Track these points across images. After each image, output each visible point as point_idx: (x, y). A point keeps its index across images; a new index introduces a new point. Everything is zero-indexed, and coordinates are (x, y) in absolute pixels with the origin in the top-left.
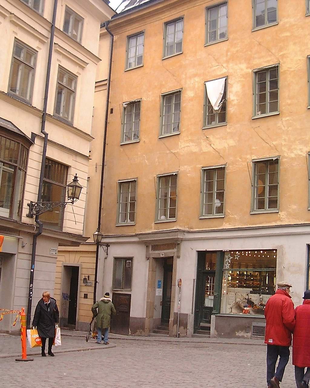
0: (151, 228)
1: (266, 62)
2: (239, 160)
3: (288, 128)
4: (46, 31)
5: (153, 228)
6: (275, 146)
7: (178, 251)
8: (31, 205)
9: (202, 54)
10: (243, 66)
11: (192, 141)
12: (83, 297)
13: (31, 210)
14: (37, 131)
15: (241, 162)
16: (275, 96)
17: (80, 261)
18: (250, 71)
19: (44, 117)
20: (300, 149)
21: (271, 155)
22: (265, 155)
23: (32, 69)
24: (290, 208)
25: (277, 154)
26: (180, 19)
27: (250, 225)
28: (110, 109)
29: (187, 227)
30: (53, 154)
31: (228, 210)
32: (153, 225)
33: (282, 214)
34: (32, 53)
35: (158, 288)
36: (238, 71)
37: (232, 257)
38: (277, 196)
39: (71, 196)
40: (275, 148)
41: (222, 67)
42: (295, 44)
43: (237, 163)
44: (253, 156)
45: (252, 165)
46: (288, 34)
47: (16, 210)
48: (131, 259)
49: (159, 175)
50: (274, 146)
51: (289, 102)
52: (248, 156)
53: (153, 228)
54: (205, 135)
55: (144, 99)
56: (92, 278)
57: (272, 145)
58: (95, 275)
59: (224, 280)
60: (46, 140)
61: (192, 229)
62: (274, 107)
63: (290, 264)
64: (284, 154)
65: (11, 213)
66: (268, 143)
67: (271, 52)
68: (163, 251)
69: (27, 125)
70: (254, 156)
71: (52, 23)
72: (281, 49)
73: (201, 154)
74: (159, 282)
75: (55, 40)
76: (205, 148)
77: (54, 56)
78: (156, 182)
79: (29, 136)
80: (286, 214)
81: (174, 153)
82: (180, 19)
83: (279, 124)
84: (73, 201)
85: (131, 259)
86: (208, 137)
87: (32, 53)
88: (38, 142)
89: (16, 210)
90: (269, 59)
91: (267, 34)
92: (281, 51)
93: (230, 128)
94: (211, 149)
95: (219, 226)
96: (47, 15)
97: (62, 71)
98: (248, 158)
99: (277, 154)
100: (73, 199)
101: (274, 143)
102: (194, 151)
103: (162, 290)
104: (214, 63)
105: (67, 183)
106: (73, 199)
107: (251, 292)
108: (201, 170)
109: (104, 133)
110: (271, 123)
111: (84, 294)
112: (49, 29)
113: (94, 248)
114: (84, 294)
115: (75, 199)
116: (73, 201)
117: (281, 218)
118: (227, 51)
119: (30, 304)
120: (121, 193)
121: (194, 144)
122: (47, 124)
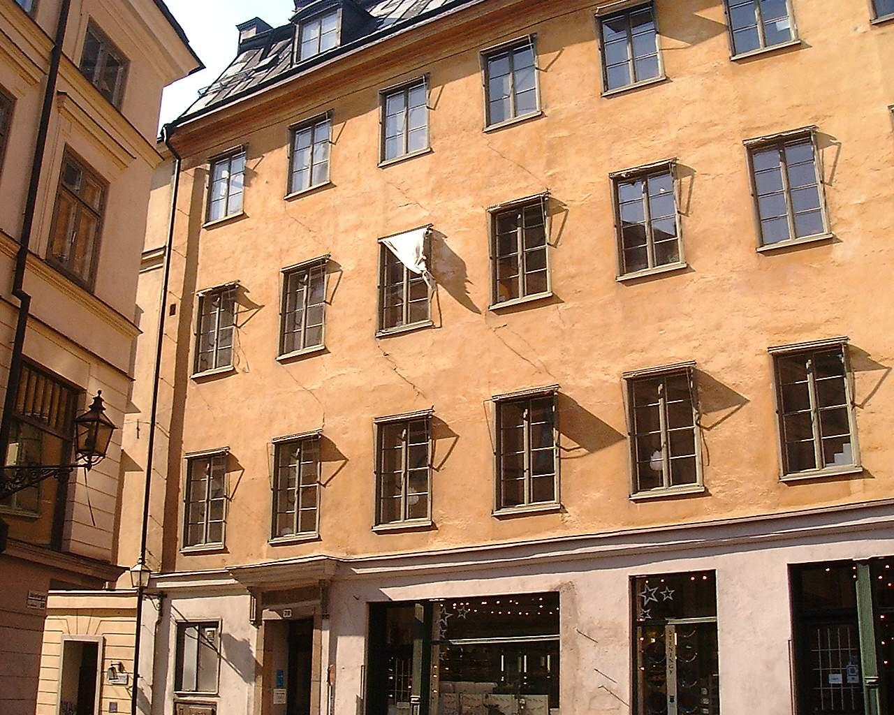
0: (260, 556)
1: (515, 191)
2: (461, 399)
3: (573, 325)
4: (42, 60)
5: (265, 554)
6: (545, 366)
7: (325, 605)
10: (466, 201)
11: (352, 363)
12: (108, 710)
15: (467, 404)
16: (537, 261)
17: (102, 630)
18: (482, 211)
20: (604, 369)
21: (537, 384)
22: (523, 384)
24: (586, 498)
25: (551, 381)
27: (492, 540)
28: (170, 306)
29: (344, 550)
31: (438, 511)
32: (266, 546)
35: (278, 687)
36: (454, 212)
37: (448, 622)
38: (559, 633)
39: (85, 448)
40: (545, 370)
41: (419, 206)
42: (578, 152)
43: (457, 406)
44: (495, 390)
45: (492, 407)
46: (564, 133)
48: (214, 624)
49: (277, 439)
50: (542, 365)
51: (573, 270)
52: (483, 391)
53: (265, 554)
54: (381, 350)
56: (129, 667)
57: (538, 364)
58: (137, 634)
59: (433, 666)
61: (354, 554)
62: (537, 282)
63: (593, 622)
64: (567, 381)
66: (528, 360)
67: (528, 171)
68: (291, 605)
70: (495, 388)
71: (56, 41)
72: (550, 163)
73: (374, 390)
74: (280, 673)
78: (271, 455)
80: (578, 512)
81: (310, 391)
84: (90, 462)
85: (214, 624)
86: (387, 353)
90: (524, 184)
92: (550, 169)
95: (420, 547)
97: (74, 167)
98: (481, 395)
99: (551, 381)
100: (90, 458)
101: (543, 358)
102: (357, 385)
103: (284, 691)
105: (78, 413)
106: (90, 458)
107: (496, 691)
108: (374, 424)
109: (151, 407)
111: (111, 703)
112: (46, 55)
113: (132, 603)
114: (111, 703)
115: (94, 458)
116: (90, 462)
117: (567, 521)
118: (430, 173)
119: (45, 113)
120: (202, 315)
121: (355, 370)
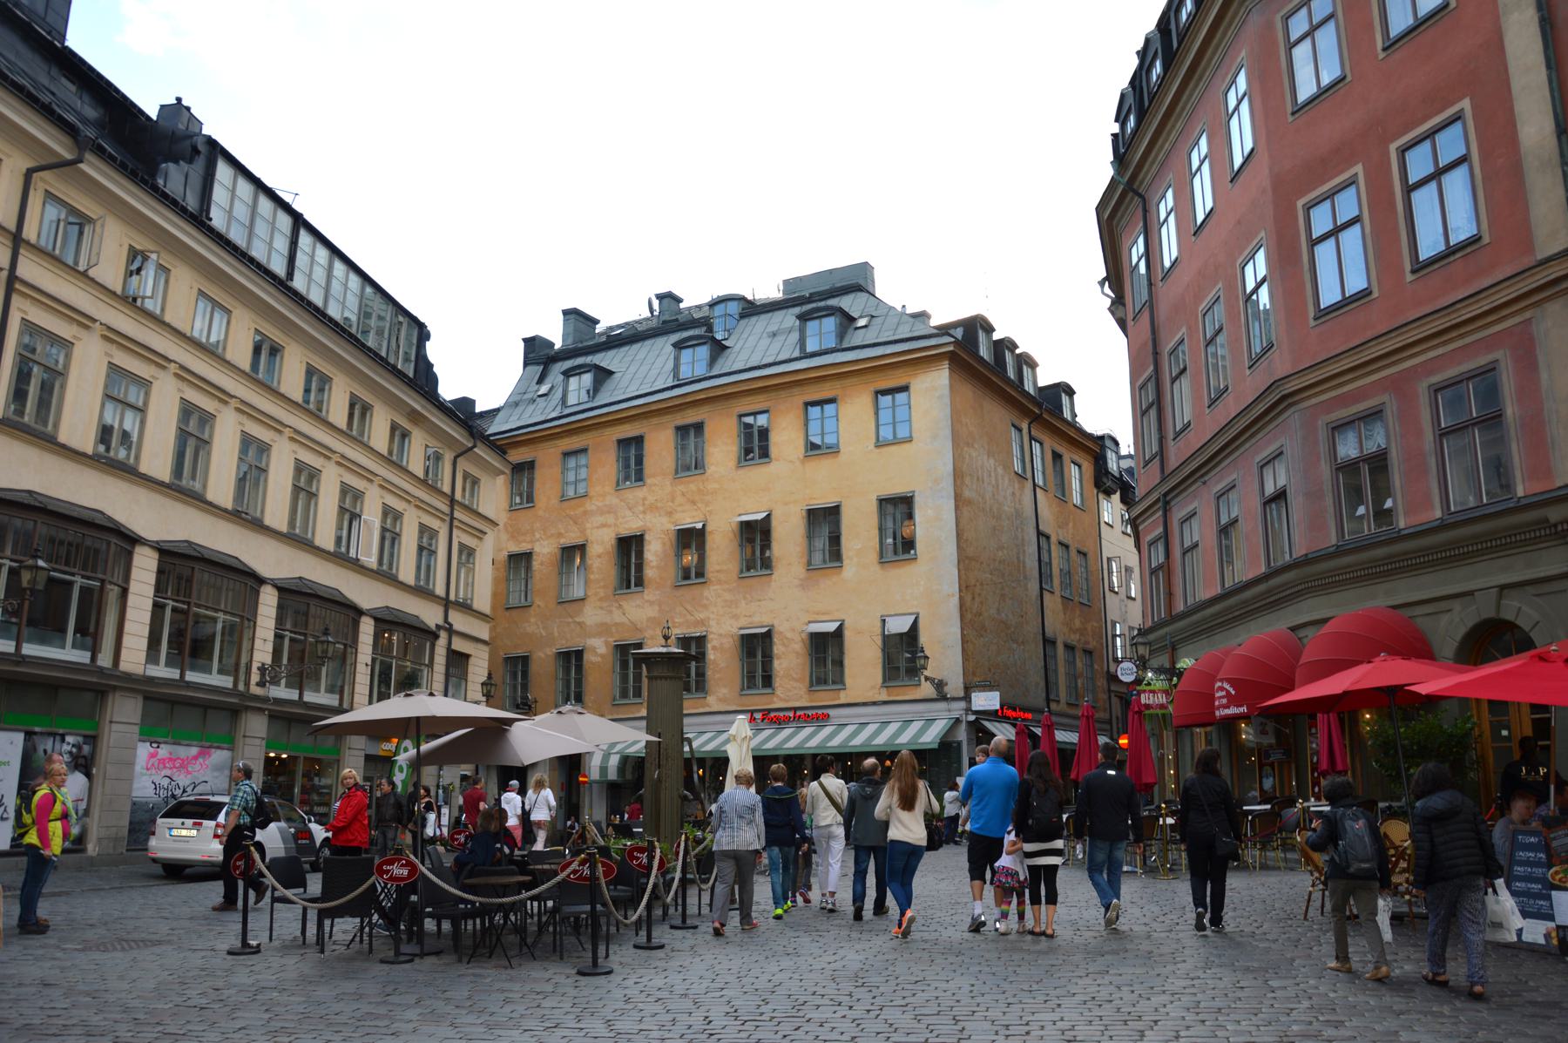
8: (262, 669)
9: (612, 500)
13: (263, 675)
14: (441, 622)
19: (447, 604)
23: (433, 553)
26: (584, 451)
30: (459, 645)
33: (711, 699)
34: (433, 534)
40: (702, 622)
47: (242, 677)
55: (537, 549)
60: (451, 631)
65: (236, 683)
69: (431, 615)
72: (707, 505)
75: (456, 514)
76: (617, 617)
77: (455, 531)
79: (433, 627)
82: (584, 451)
83: (706, 593)
87: (433, 534)
88: (443, 635)
89: (242, 677)
91: (692, 485)
93: (650, 594)
94: (624, 620)
96: (447, 489)
104: (628, 513)
110: (696, 590)
122: (451, 613)
